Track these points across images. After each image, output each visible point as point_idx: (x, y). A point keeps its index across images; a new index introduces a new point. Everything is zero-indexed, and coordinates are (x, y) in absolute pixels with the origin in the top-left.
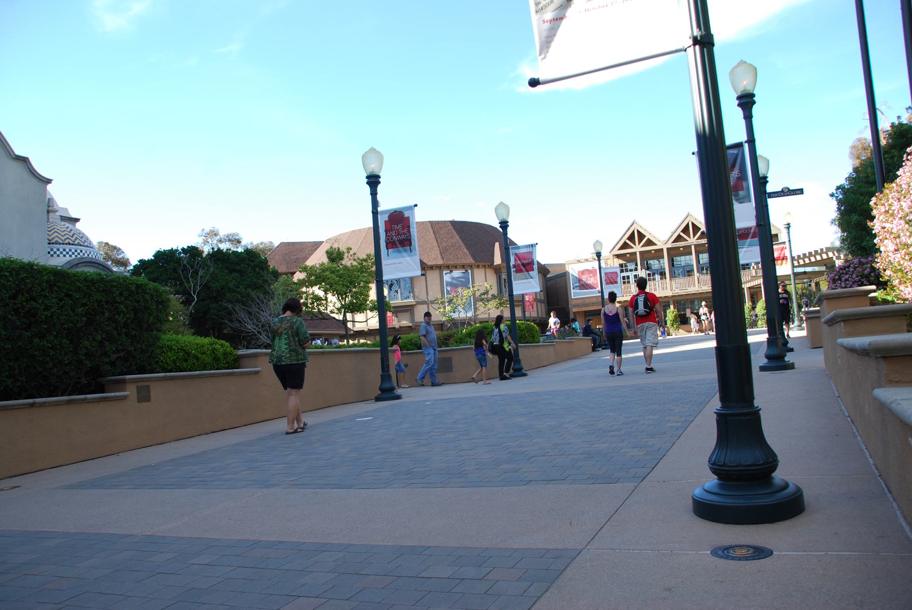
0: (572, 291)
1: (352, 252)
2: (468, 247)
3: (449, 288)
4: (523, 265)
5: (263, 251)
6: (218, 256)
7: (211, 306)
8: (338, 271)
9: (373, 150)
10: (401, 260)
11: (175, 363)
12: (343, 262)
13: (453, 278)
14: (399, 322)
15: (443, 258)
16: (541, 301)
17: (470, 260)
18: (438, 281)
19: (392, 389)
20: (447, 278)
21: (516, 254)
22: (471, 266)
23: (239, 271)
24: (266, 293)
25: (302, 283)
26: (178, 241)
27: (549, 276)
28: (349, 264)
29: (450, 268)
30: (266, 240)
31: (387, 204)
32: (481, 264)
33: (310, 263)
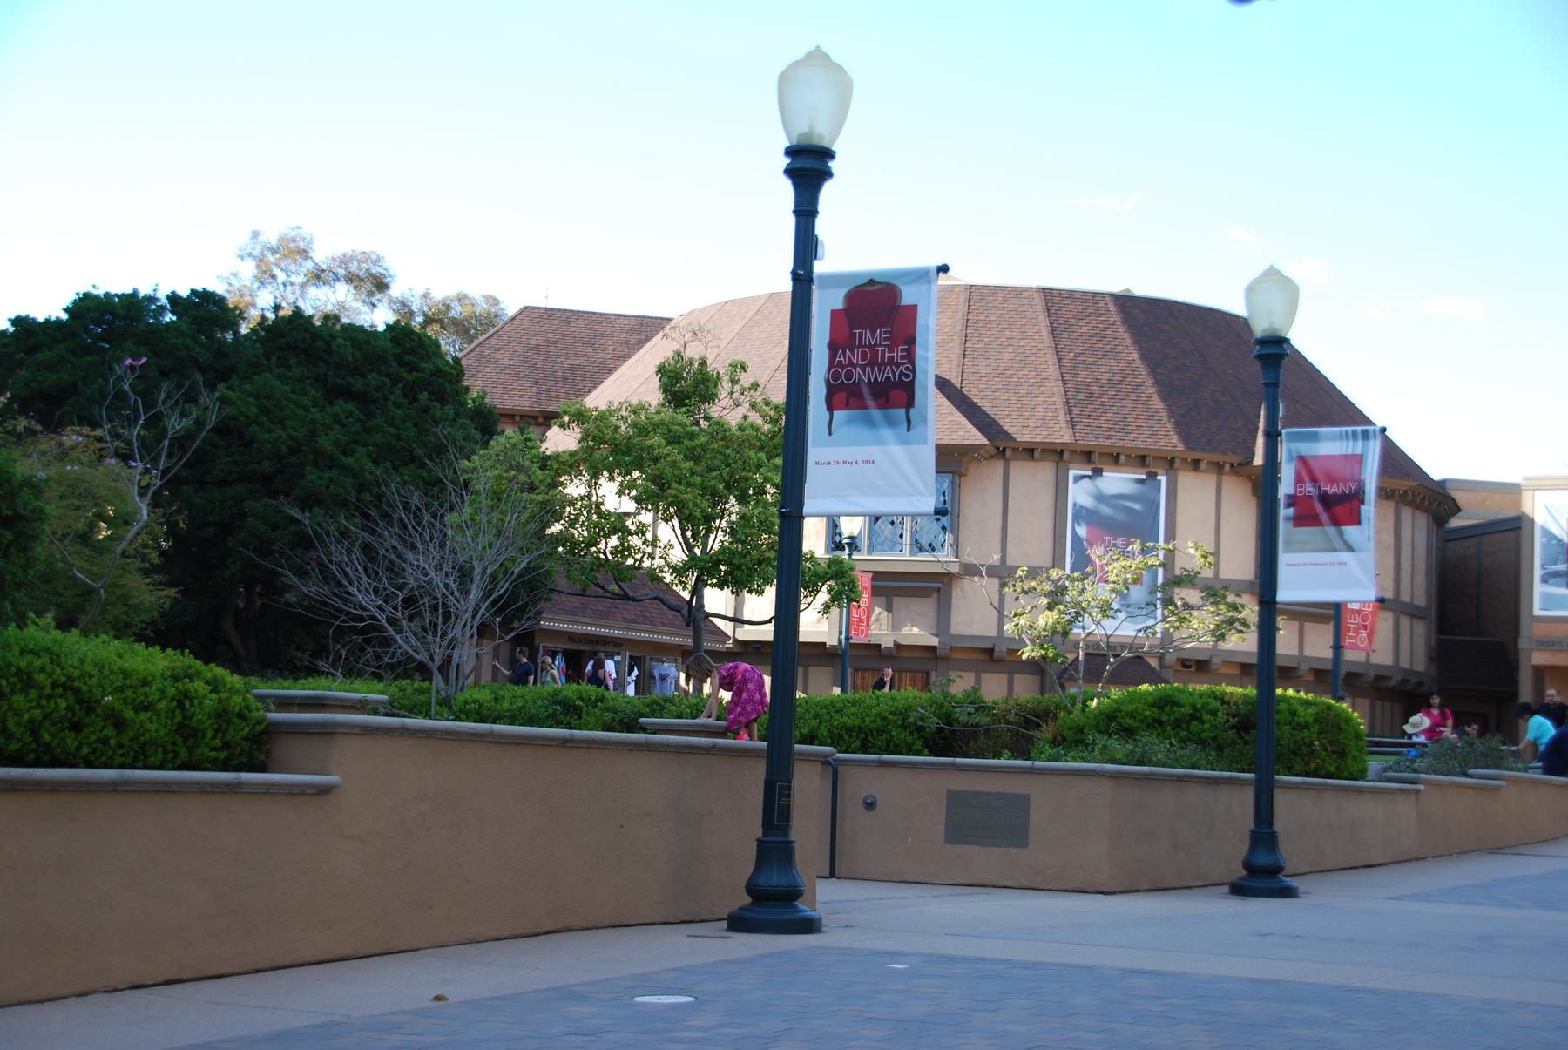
0: (1539, 588)
1: (745, 380)
2: (1168, 393)
3: (1082, 531)
4: (1325, 500)
5: (463, 328)
6: (294, 336)
7: (250, 505)
8: (692, 436)
9: (818, 57)
10: (874, 451)
11: (34, 733)
12: (714, 411)
13: (1100, 497)
14: (895, 626)
15: (1072, 423)
16: (1413, 612)
17: (1168, 440)
18: (1046, 500)
19: (791, 895)
20: (1080, 493)
21: (1302, 459)
22: (1169, 463)
23: (363, 399)
24: (433, 484)
25: (569, 464)
26: (160, 269)
27: (1455, 523)
28: (733, 419)
29: (1095, 459)
30: (476, 291)
31: (848, 251)
32: (1206, 457)
33: (597, 400)
